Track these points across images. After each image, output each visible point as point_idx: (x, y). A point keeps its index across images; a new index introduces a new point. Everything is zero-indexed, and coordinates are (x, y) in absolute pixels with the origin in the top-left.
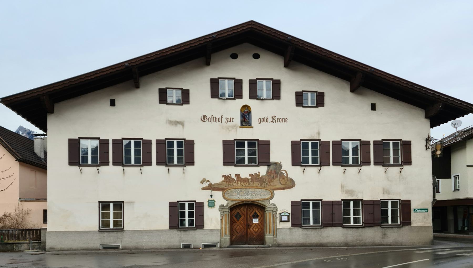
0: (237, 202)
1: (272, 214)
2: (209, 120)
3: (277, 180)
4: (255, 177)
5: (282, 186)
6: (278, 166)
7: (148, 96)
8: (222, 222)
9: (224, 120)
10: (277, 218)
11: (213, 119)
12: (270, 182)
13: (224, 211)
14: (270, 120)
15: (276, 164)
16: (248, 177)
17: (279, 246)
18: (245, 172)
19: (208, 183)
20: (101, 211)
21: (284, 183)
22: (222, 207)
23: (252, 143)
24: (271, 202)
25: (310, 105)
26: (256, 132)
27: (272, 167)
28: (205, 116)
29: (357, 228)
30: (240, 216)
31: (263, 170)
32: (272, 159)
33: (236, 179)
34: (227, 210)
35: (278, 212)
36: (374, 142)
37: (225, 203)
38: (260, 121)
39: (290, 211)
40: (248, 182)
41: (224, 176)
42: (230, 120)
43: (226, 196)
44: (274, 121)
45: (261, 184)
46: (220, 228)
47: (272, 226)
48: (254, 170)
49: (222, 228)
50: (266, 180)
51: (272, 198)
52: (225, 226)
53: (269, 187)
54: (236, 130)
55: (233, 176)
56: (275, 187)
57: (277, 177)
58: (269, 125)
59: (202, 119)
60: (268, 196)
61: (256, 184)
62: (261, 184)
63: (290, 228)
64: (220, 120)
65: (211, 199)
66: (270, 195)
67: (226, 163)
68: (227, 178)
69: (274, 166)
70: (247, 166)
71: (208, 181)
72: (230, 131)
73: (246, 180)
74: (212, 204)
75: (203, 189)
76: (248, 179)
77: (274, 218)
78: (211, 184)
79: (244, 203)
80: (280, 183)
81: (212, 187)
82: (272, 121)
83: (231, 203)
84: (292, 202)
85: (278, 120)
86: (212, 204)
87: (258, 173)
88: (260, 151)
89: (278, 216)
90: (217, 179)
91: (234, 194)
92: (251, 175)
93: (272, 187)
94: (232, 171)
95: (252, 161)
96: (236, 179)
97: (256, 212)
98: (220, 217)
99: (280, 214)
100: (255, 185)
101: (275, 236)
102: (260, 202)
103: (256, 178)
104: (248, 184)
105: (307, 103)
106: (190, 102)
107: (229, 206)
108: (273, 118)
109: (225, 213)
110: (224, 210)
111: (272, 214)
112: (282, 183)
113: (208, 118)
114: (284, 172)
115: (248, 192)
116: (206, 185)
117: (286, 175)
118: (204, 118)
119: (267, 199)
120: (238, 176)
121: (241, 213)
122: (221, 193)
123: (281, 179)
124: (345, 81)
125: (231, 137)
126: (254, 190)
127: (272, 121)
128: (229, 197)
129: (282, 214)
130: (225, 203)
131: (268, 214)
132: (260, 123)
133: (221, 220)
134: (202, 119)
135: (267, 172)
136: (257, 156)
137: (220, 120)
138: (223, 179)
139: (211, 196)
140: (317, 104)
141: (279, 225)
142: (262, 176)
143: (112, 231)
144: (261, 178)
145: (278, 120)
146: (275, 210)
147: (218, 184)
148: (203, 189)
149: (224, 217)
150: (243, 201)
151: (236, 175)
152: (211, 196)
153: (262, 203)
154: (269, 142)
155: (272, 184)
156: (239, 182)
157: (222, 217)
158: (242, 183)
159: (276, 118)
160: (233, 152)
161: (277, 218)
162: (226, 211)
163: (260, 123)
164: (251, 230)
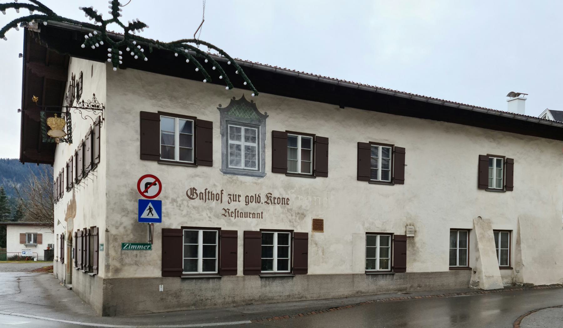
2: (201, 196)
9: (225, 198)
14: (263, 199)
20: (500, 249)
25: (299, 171)
28: (194, 189)
29: (384, 275)
36: (245, 233)
44: (270, 202)
59: (189, 194)
82: (266, 202)
85: (276, 201)
105: (295, 169)
106: (214, 165)
108: (268, 197)
113: (198, 192)
124: (438, 123)
127: (266, 202)
134: (189, 194)
136: (217, 244)
140: (195, 161)
143: (200, 278)
145: (276, 201)
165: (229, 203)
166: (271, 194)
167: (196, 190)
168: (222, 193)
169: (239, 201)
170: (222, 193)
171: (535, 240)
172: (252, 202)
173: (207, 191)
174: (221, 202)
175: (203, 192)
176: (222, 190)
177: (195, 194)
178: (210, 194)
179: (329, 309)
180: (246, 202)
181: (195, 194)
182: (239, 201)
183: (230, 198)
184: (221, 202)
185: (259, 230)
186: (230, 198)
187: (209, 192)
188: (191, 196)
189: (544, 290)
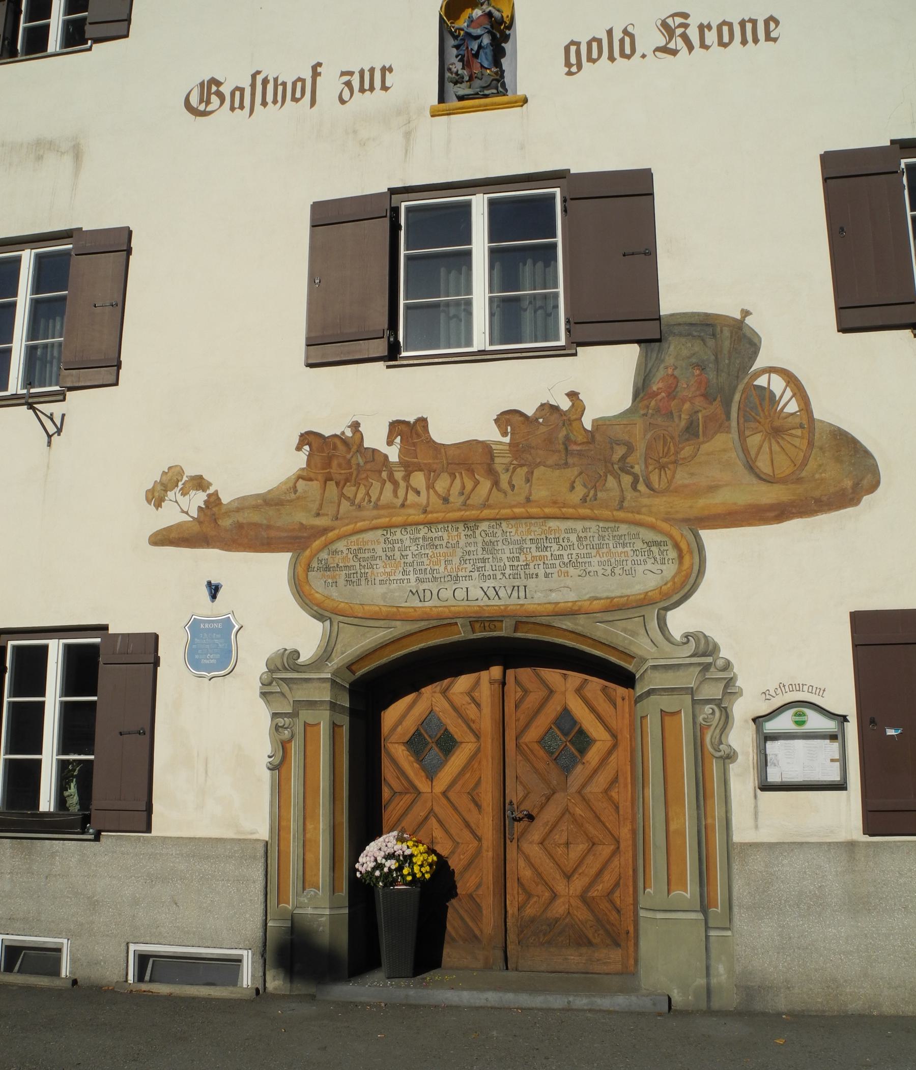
0: (400, 628)
1: (684, 719)
2: (238, 100)
3: (723, 443)
4: (542, 435)
5: (769, 495)
6: (726, 342)
7: (595, 703)
8: (279, 790)
9: (330, 85)
10: (730, 757)
11: (265, 91)
12: (664, 458)
13: (299, 705)
14: (649, 38)
15: (703, 326)
16: (491, 434)
17: (572, 1010)
18: (463, 398)
19: (199, 498)
21: (784, 467)
22: (284, 670)
23: (523, 211)
24: (680, 621)
26: (552, 126)
27: (676, 350)
30: (448, 744)
31: (603, 380)
32: (673, 300)
33: (393, 454)
34: (324, 694)
35: (743, 709)
37: (307, 636)
38: (575, 57)
39: (842, 695)
40: (491, 472)
41: (308, 439)
42: (368, 80)
43: (318, 584)
44: (680, 43)
45: (595, 484)
46: (263, 832)
47: (687, 822)
48: (532, 383)
49: (279, 826)
50: (630, 449)
51: (684, 587)
52: (306, 815)
53: (660, 503)
54: (408, 135)
55: (375, 437)
56: (703, 504)
57: (720, 424)
58: (648, 72)
59: (194, 101)
60: (650, 575)
61: (549, 483)
62: (595, 484)
63: (851, 845)
64: (304, 89)
65: (205, 609)
66: (670, 570)
67: (331, 342)
68: (333, 457)
69: (697, 347)
70: (482, 357)
71: (199, 483)
72: (363, 144)
73: (471, 458)
74: (213, 648)
75: (166, 538)
76: (486, 448)
77: (710, 759)
78: (213, 501)
79: (462, 634)
80: (751, 468)
81: (220, 527)
82: (664, 49)
83: (356, 643)
84: (828, 159)
85: (711, 37)
86: (213, 648)
87: (565, 405)
88: (582, 245)
89: (741, 738)
90: (258, 463)
91: (380, 569)
92: (508, 419)
93: (683, 506)
94: (369, 399)
95: (510, 321)
96: (393, 454)
97: (566, 713)
98: (268, 749)
99: (757, 720)
100: (540, 493)
101: (717, 910)
102: (581, 624)
103: (549, 440)
104: (485, 485)
107: (337, 661)
109: (306, 715)
110: (302, 694)
111: (684, 719)
112: (763, 465)
113: (226, 90)
114: (777, 385)
115: (489, 547)
116: (182, 509)
117: (793, 407)
118: (206, 97)
119: (644, 602)
120: (410, 432)
121: (456, 729)
122: (279, 563)
123: (754, 441)
125: (370, 179)
126: (537, 530)
128: (337, 594)
129: (771, 726)
130: (307, 636)
131: (652, 725)
132: (572, 66)
133: (278, 767)
135: (641, 390)
137: (304, 89)
138: (300, 460)
139: (214, 590)
141: (755, 820)
142: (599, 424)
144: (591, 437)
145: (711, 37)
146: (712, 691)
147: (269, 501)
148: (166, 538)
149: (295, 749)
150: (446, 623)
151: (397, 428)
152: (214, 590)
153: (601, 631)
154: (645, 176)
155: (682, 477)
156: (419, 480)
157: (284, 746)
158: (442, 485)
159: (693, 22)
160: (384, 270)
161: (730, 757)
162: (311, 704)
163: (572, 66)
164: (534, 851)
165: (342, 101)
166: (685, 16)
167: (218, 84)
168: (315, 74)
169: (384, 88)
170: (315, 74)
171: (522, 148)
172: (294, 99)
173: (259, 79)
174: (313, 102)
175: (246, 84)
176: (319, 64)
177: (214, 98)
178: (270, 88)
179: (382, 647)
180: (568, 64)
181: (214, 98)
182: (384, 88)
183: (348, 84)
184: (313, 102)
185: (889, 144)
186: (348, 84)
187: (265, 82)
188: (202, 107)
189: (771, 508)
